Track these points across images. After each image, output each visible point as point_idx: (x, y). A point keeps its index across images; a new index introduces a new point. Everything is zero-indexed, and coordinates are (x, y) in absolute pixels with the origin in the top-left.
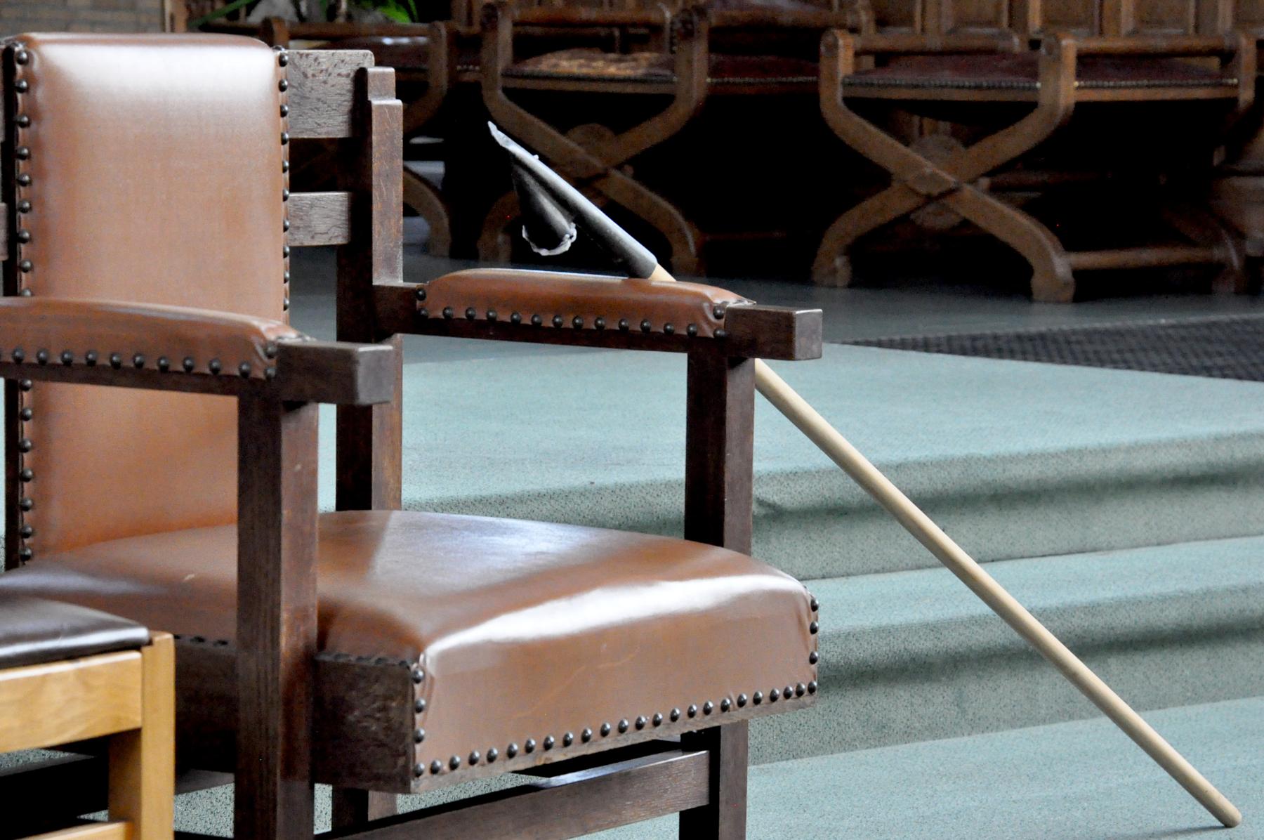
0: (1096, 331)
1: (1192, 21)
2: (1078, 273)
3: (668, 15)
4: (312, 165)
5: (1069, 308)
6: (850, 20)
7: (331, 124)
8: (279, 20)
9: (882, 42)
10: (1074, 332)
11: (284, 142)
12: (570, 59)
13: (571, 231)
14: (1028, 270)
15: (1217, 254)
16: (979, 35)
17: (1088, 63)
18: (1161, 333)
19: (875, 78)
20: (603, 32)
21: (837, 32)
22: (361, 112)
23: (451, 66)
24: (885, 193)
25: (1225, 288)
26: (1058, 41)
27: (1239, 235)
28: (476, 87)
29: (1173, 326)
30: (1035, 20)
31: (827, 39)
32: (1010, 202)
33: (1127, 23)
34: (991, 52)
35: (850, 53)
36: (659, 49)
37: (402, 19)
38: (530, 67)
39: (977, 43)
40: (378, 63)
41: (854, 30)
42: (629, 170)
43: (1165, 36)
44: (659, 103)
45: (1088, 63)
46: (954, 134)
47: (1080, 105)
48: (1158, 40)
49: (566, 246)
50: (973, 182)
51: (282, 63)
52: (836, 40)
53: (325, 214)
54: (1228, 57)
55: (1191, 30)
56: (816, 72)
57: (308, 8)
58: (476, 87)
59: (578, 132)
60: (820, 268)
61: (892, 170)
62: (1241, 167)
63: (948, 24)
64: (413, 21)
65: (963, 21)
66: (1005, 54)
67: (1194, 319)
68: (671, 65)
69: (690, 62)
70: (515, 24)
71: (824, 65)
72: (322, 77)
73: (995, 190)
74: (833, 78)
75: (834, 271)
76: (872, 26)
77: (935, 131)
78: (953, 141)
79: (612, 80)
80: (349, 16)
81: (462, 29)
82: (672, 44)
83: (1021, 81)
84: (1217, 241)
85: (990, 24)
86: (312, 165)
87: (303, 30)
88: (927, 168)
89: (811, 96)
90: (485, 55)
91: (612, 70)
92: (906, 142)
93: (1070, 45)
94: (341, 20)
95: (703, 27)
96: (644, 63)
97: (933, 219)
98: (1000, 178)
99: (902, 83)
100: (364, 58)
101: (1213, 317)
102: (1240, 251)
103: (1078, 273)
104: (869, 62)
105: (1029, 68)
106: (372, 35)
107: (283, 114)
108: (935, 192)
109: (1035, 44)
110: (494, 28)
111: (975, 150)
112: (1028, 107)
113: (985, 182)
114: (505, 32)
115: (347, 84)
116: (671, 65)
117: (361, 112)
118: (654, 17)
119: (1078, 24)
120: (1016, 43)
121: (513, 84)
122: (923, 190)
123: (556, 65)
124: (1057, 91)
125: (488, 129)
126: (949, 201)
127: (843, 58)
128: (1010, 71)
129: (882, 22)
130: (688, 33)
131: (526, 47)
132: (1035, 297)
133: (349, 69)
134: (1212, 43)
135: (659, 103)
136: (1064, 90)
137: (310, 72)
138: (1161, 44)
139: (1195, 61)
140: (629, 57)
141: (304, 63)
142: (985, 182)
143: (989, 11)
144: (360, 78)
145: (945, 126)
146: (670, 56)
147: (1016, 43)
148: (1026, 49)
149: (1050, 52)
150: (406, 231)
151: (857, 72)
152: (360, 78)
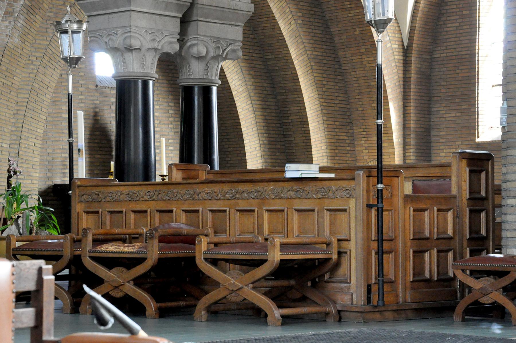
0: (289, 337)
1: (316, 233)
2: (283, 317)
3: (145, 230)
4: (23, 298)
5: (280, 328)
6: (205, 232)
7: (30, 286)
8: (13, 235)
9: (216, 240)
10: (282, 337)
11: (13, 292)
12: (111, 246)
13: (111, 321)
14: (266, 316)
15: (328, 309)
16: (247, 237)
17: (284, 246)
18: (310, 337)
19: (214, 251)
20: (123, 237)
21: (201, 236)
22: (40, 281)
23: (71, 249)
24: (219, 289)
25: (330, 320)
26: (274, 239)
27: (334, 302)
28: (80, 256)
29: (314, 335)
30: (266, 232)
31: (197, 239)
32: (259, 292)
33: (296, 233)
34: (252, 242)
35: (206, 243)
36: (142, 242)
37: (55, 233)
38: (98, 249)
39: (247, 240)
40: (47, 264)
41: (206, 235)
42: (132, 283)
43: (308, 238)
44: (140, 261)
45: (284, 246)
46: (240, 270)
47: (281, 260)
48: (306, 239)
49: (110, 325)
50: (247, 286)
51: (13, 266)
52: (201, 239)
53: (27, 314)
54: (328, 244)
55: (316, 236)
56: (194, 249)
57: (22, 230)
58: (80, 256)
59: (114, 270)
60: (196, 314)
61: (220, 281)
62: (333, 280)
63: (237, 233)
64: (59, 234)
65: (242, 232)
66: (257, 243)
67: (321, 332)
68: (146, 248)
69: (152, 246)
70: (93, 235)
71: (197, 247)
72: (26, 270)
73: (254, 288)
74: (200, 251)
75: (202, 316)
76: (213, 234)
77: (234, 269)
78: (240, 272)
79: (127, 253)
80: (37, 233)
81: (75, 237)
82: (146, 240)
83: (263, 252)
84: (327, 305)
85: (251, 233)
86: (23, 298)
87: (21, 239)
88: (232, 282)
89: (193, 259)
90: (83, 245)
91: (126, 249)
92: (225, 272)
93: (278, 241)
94: (34, 234)
95: (157, 235)
96: (136, 247)
97: (234, 298)
98: (256, 284)
99: (222, 253)
100: (41, 263)
101: (327, 331)
102: (335, 307)
103: (283, 317)
104: (212, 246)
105: (265, 248)
106: (44, 239)
107: (13, 274)
108: (234, 289)
109: (266, 240)
110: (86, 236)
111: (248, 275)
112: (263, 262)
113: (251, 286)
114: (90, 238)
115: (35, 272)
116: (146, 248)
117: (40, 281)
118: (140, 231)
119: (280, 233)
120: (260, 239)
121: (93, 255)
122: (231, 289)
123: (107, 248)
124: (274, 257)
125: (83, 289)
126: (238, 292)
127: (203, 246)
128: (258, 249)
129: (216, 232)
130: (152, 238)
131: (97, 242)
132: (269, 324)
133: (36, 267)
134: (324, 240)
135: (140, 261)
136: (276, 256)
137: (23, 269)
138: (307, 240)
139: (318, 246)
140: (131, 245)
141: (21, 266)
142: (251, 286)
143: (251, 229)
144: (40, 270)
145: (238, 267)
146: (146, 244)
147: (260, 239)
148: (263, 241)
149: (271, 243)
150: (55, 304)
151: (208, 249)
152: (40, 270)
